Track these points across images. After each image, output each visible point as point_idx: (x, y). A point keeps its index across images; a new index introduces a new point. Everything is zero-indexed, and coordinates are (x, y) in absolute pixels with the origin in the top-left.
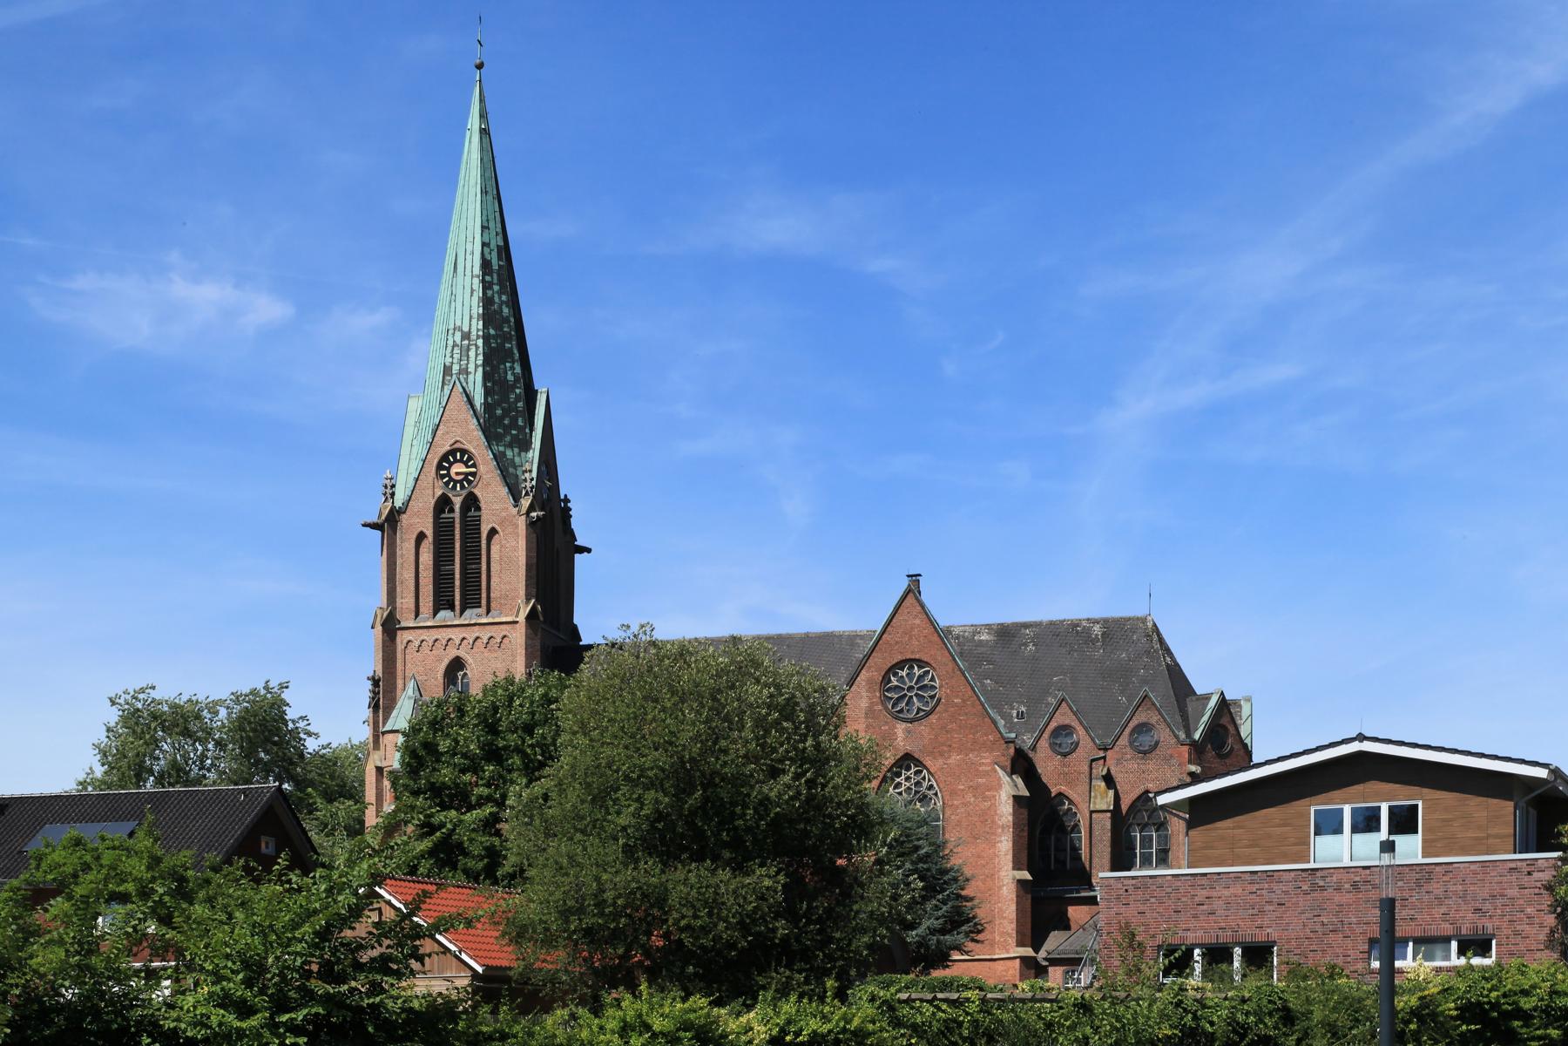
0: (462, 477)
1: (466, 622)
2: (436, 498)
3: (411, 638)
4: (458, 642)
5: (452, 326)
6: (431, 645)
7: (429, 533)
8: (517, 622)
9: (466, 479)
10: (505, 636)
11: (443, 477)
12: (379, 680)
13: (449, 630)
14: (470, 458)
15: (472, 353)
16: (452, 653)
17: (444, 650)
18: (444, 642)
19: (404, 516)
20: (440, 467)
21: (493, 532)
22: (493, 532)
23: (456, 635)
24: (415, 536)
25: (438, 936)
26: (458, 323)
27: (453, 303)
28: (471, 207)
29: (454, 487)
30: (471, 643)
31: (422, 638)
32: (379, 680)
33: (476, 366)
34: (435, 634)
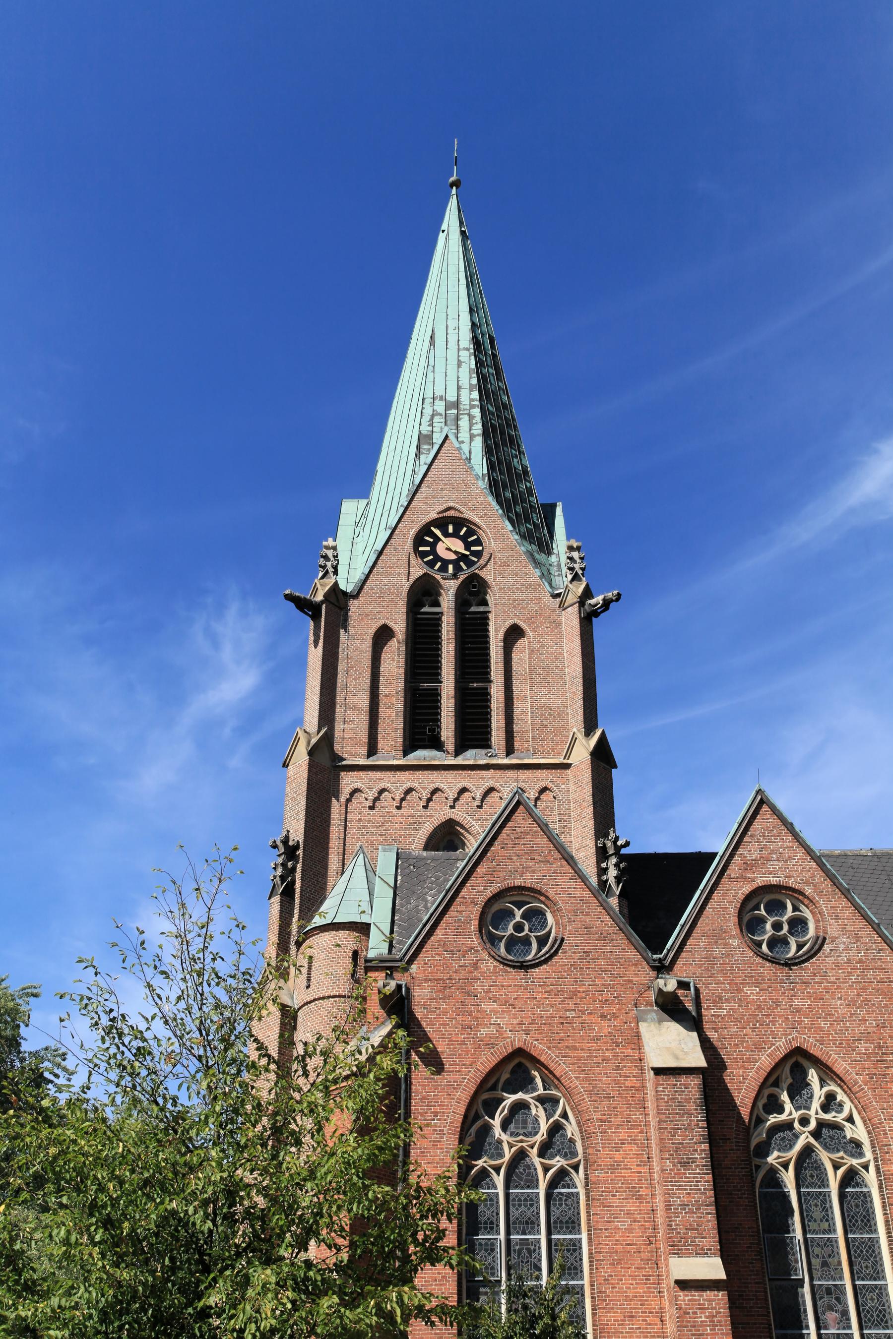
0: (453, 557)
1: (471, 762)
2: (412, 580)
3: (358, 785)
4: (452, 795)
5: (429, 395)
6: (398, 798)
7: (400, 627)
8: (567, 766)
9: (456, 563)
10: (544, 790)
11: (423, 555)
12: (296, 847)
13: (435, 774)
14: (471, 532)
15: (464, 423)
16: (440, 813)
17: (425, 807)
18: (425, 795)
19: (356, 602)
20: (419, 540)
21: (514, 634)
22: (514, 634)
23: (450, 783)
24: (372, 631)
25: (198, 1334)
26: (440, 392)
27: (430, 375)
28: (452, 296)
29: (444, 569)
30: (479, 797)
31: (382, 785)
32: (296, 847)
33: (472, 437)
34: (407, 780)
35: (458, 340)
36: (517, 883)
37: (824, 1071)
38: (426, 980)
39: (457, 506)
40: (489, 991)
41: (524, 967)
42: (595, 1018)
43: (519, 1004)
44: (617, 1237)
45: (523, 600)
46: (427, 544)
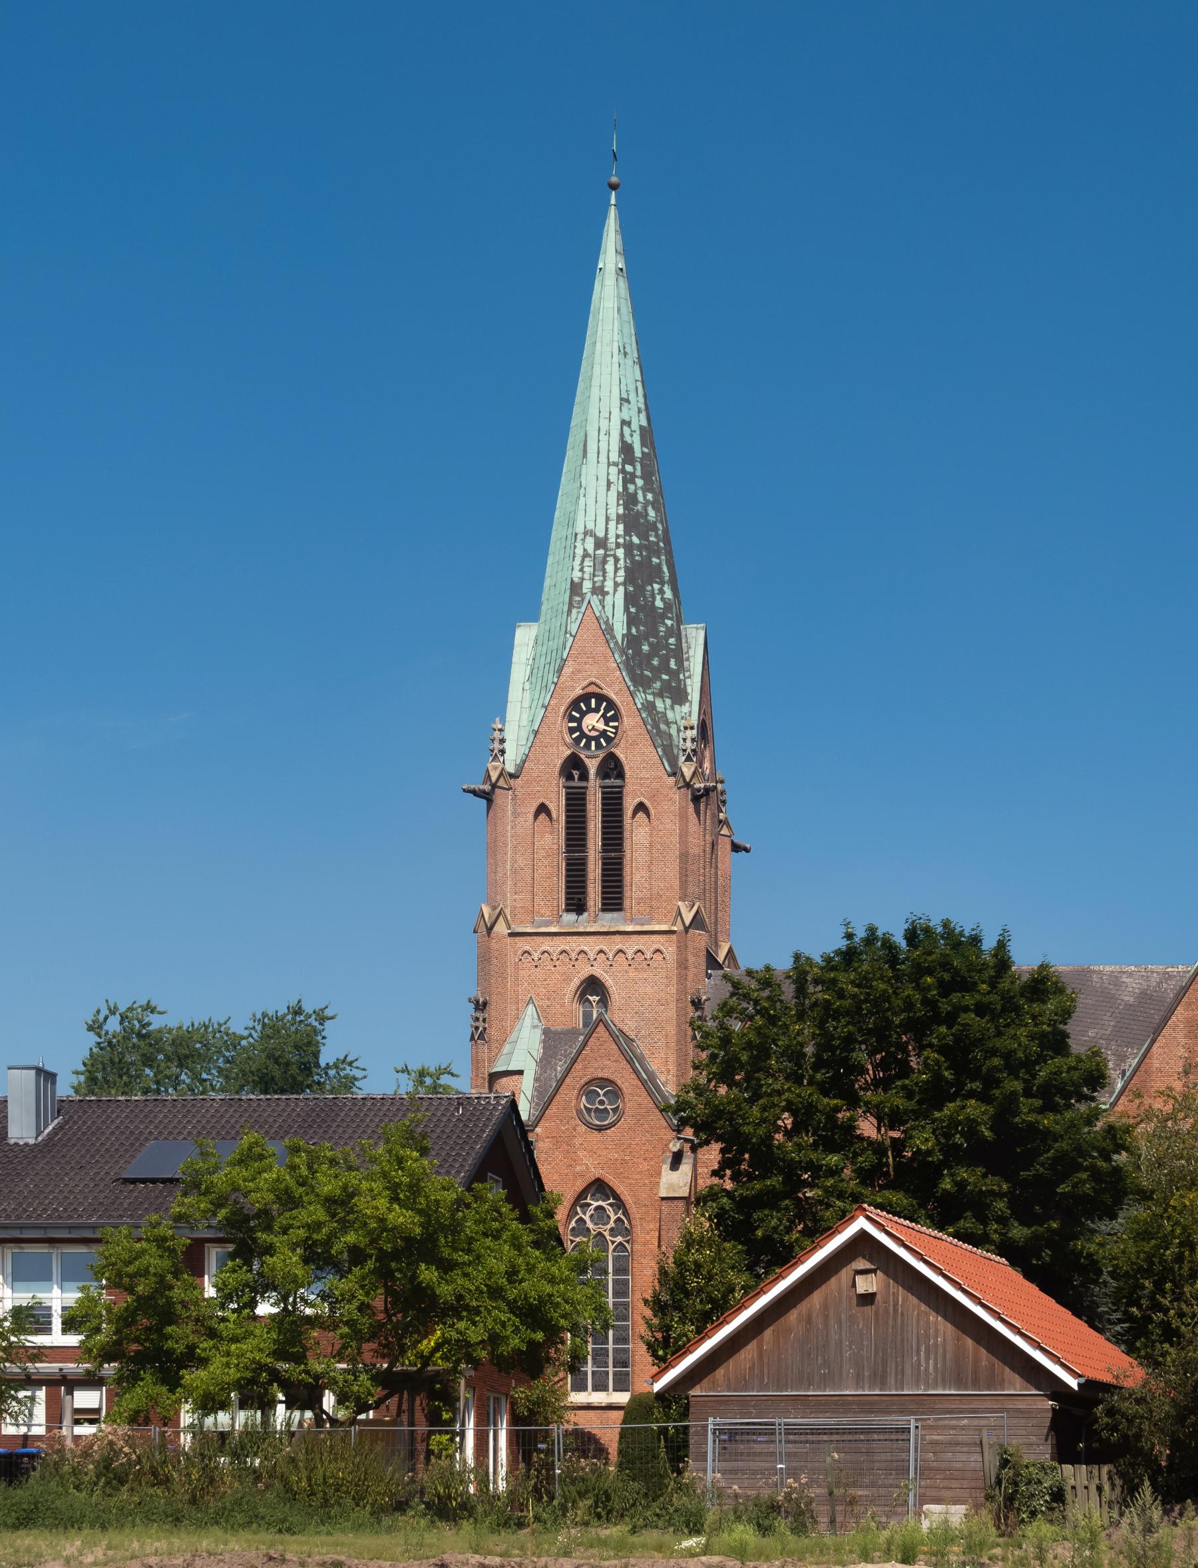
13: (581, 939)
29: (587, 746)
33: (616, 585)
35: (609, 451)
36: (600, 1075)
37: (621, 1269)
38: (548, 1137)
39: (598, 682)
40: (582, 1144)
41: (600, 1129)
42: (640, 1160)
43: (599, 1152)
44: (645, 1279)
45: (648, 779)
46: (579, 710)
